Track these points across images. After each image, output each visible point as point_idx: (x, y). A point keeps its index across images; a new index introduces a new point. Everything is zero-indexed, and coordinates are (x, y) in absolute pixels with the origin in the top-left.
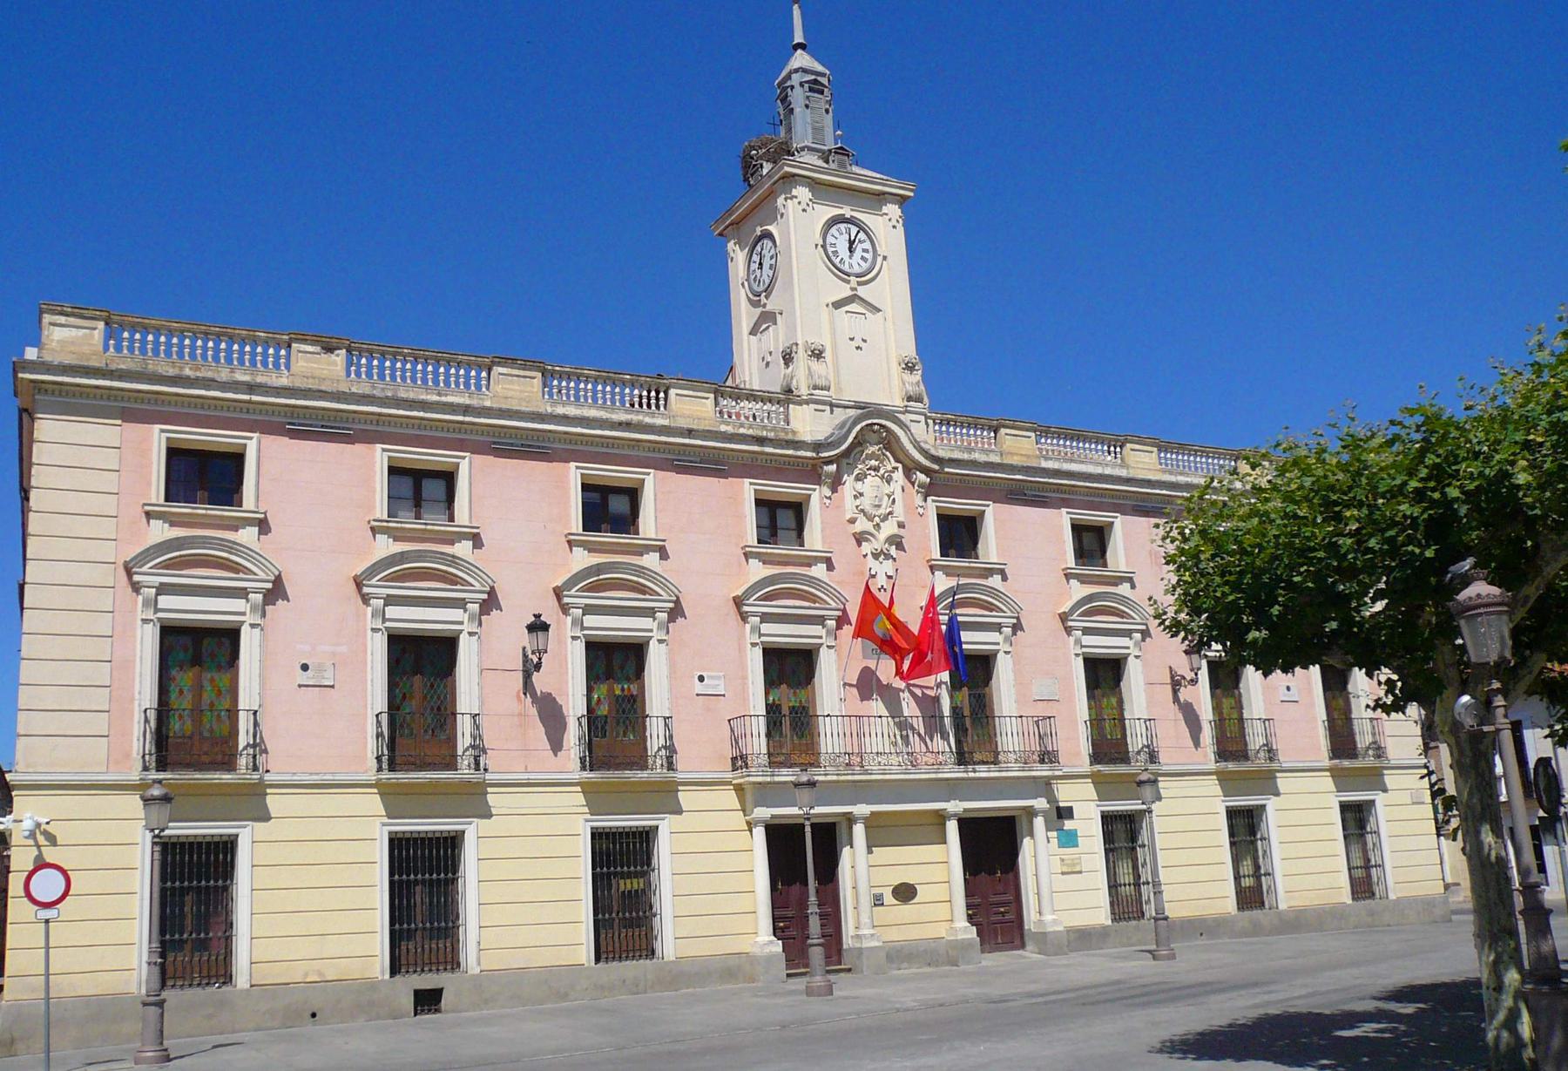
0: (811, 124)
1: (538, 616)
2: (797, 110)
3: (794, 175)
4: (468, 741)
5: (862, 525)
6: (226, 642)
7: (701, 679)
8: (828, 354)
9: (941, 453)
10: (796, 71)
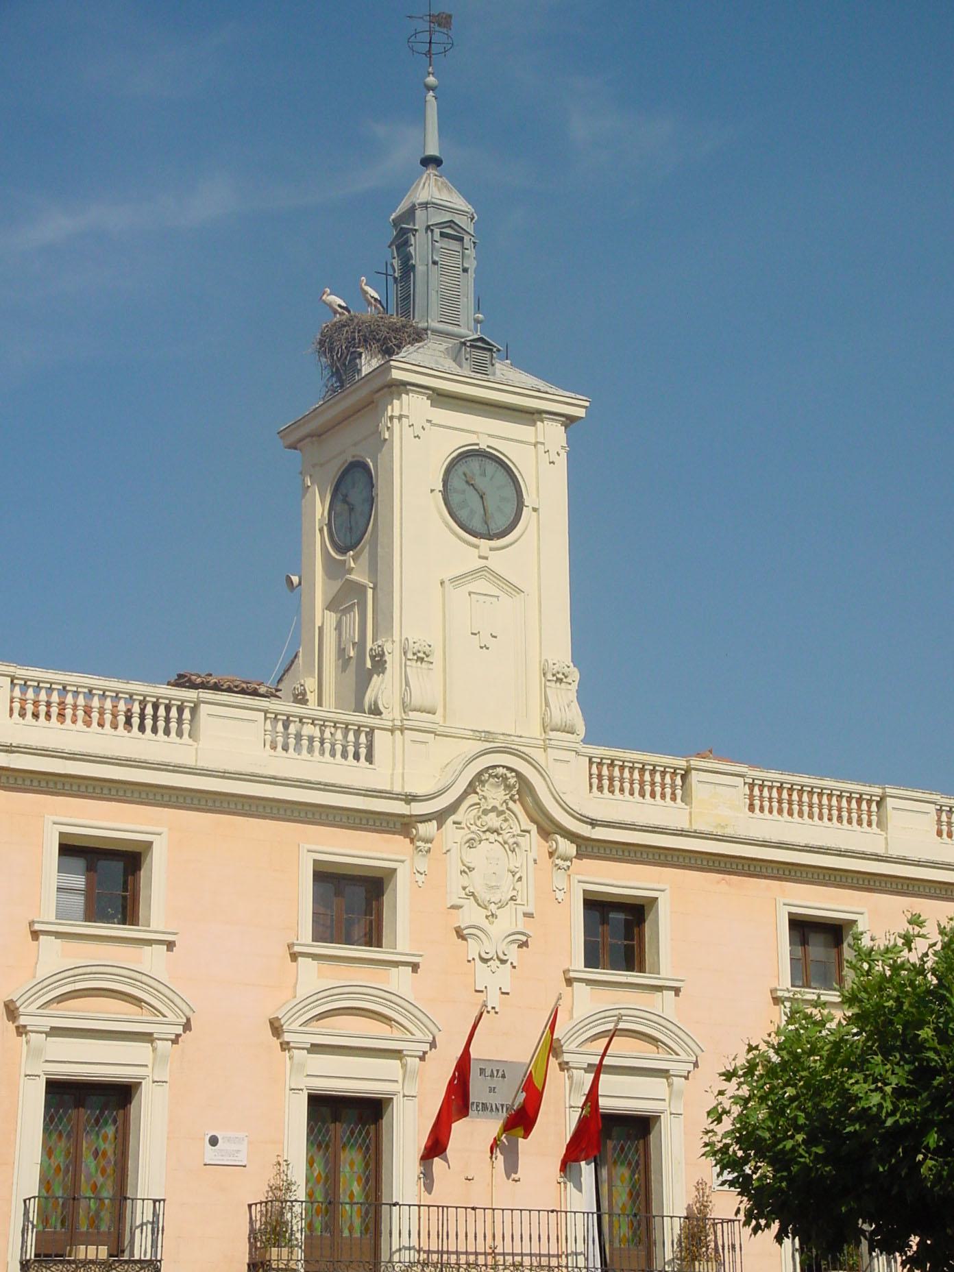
0: (449, 289)
2: (420, 269)
3: (405, 384)
5: (471, 915)
7: (214, 1141)
8: (437, 658)
10: (425, 205)
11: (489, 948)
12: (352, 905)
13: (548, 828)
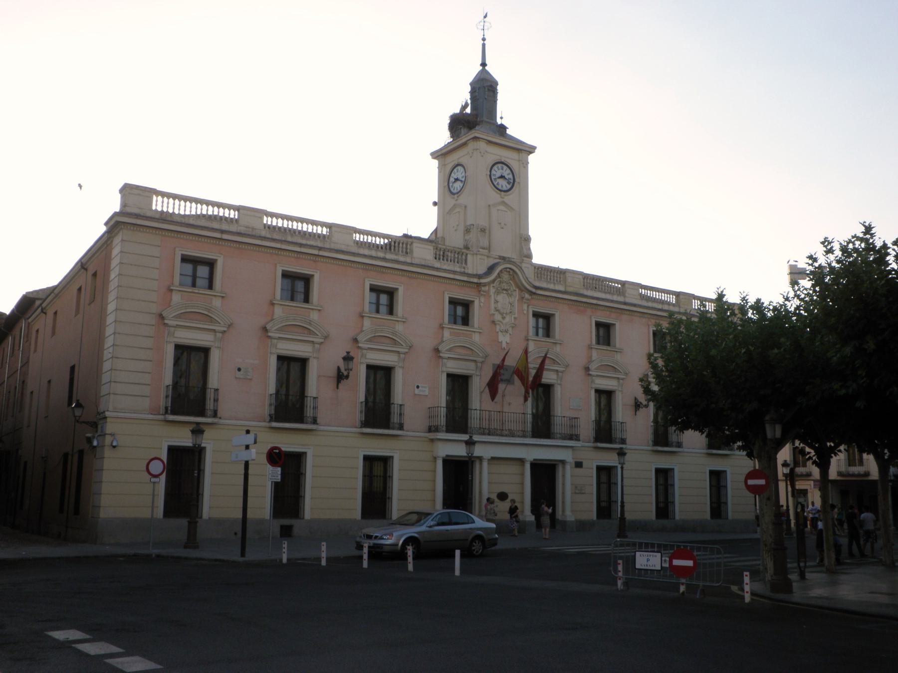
1: (348, 353)
4: (212, 408)
6: (202, 355)
7: (418, 387)
8: (487, 231)
9: (537, 284)
11: (503, 328)
12: (461, 312)
13: (522, 289)
